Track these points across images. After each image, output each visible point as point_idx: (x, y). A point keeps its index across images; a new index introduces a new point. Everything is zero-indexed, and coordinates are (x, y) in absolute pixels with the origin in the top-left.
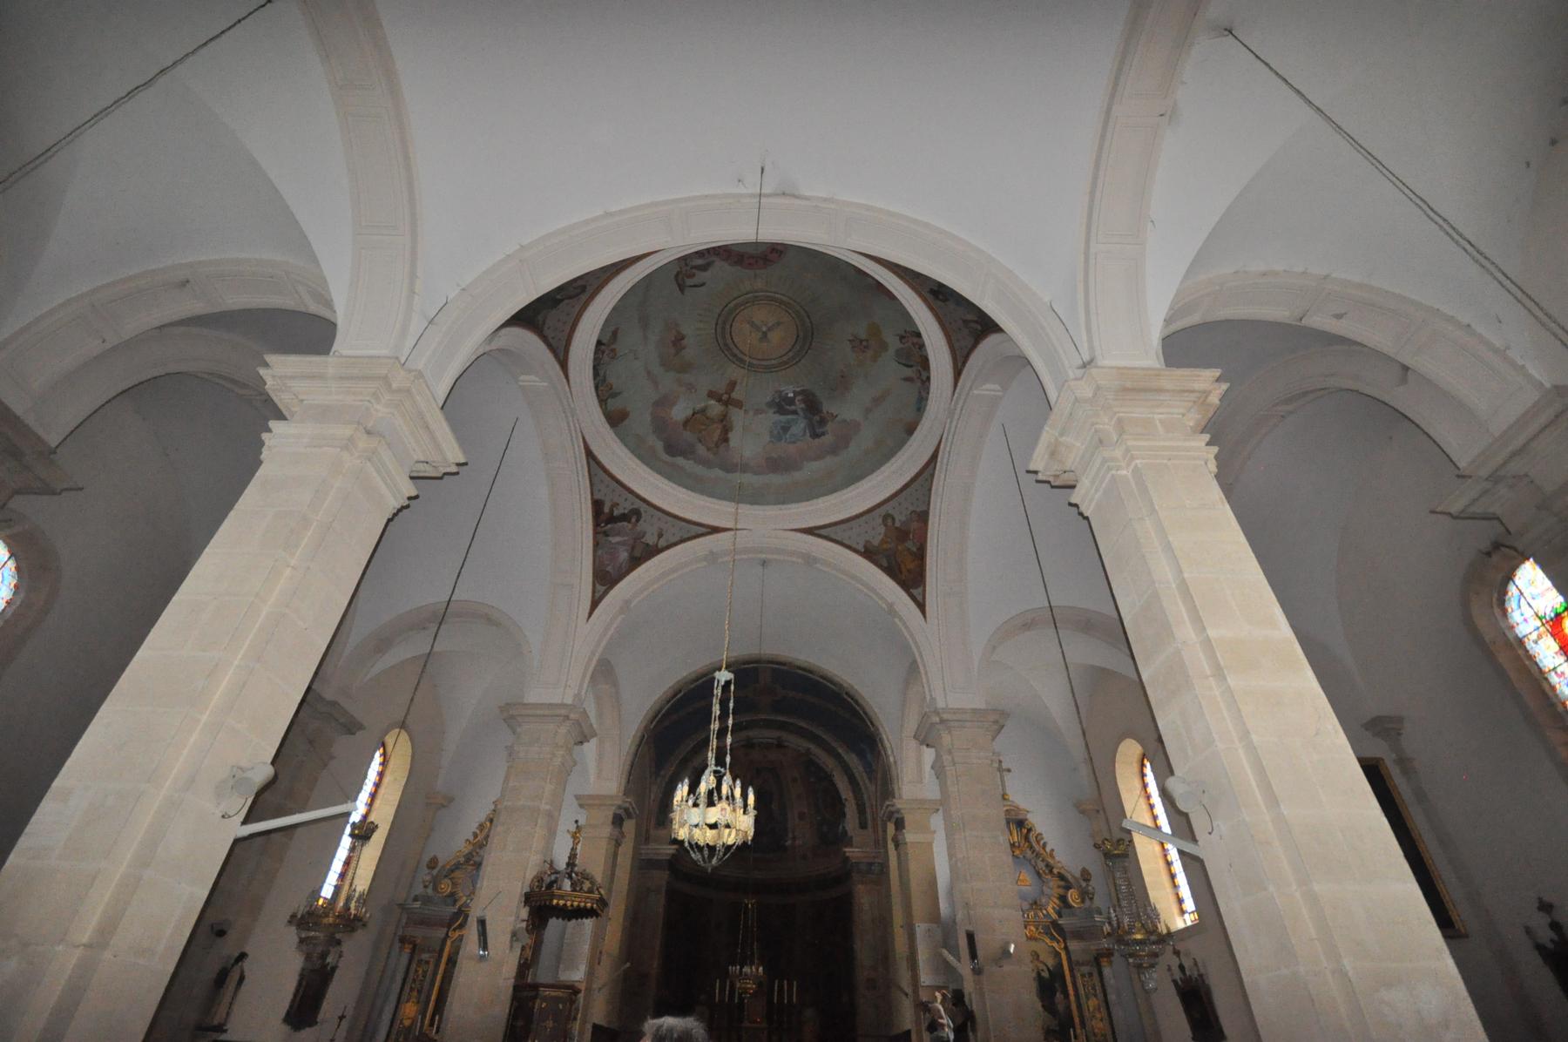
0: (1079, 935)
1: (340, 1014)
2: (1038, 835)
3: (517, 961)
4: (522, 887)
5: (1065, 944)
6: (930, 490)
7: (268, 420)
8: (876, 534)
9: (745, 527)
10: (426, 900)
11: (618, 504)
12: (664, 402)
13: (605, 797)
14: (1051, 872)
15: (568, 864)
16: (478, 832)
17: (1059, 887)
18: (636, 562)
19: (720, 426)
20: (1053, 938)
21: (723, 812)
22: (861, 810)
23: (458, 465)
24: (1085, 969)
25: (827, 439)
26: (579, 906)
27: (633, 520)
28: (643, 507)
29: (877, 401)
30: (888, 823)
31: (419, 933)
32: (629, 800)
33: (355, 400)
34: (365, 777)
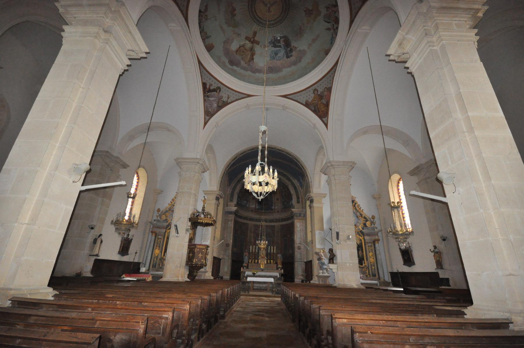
0: (368, 235)
1: (136, 252)
2: (358, 205)
3: (189, 237)
4: (188, 216)
5: (364, 237)
6: (333, 78)
7: (62, 26)
8: (310, 97)
9: (261, 95)
10: (158, 221)
11: (212, 85)
12: (227, 42)
13: (214, 191)
14: (362, 216)
15: (202, 210)
16: (172, 201)
17: (364, 221)
18: (220, 108)
20: (360, 235)
21: (266, 177)
22: (298, 198)
23: (147, 53)
24: (370, 244)
25: (293, 59)
26: (207, 222)
27: (218, 91)
28: (222, 86)
29: (314, 40)
30: (307, 201)
31: (157, 230)
32: (221, 192)
33: (97, 17)
34: (132, 183)
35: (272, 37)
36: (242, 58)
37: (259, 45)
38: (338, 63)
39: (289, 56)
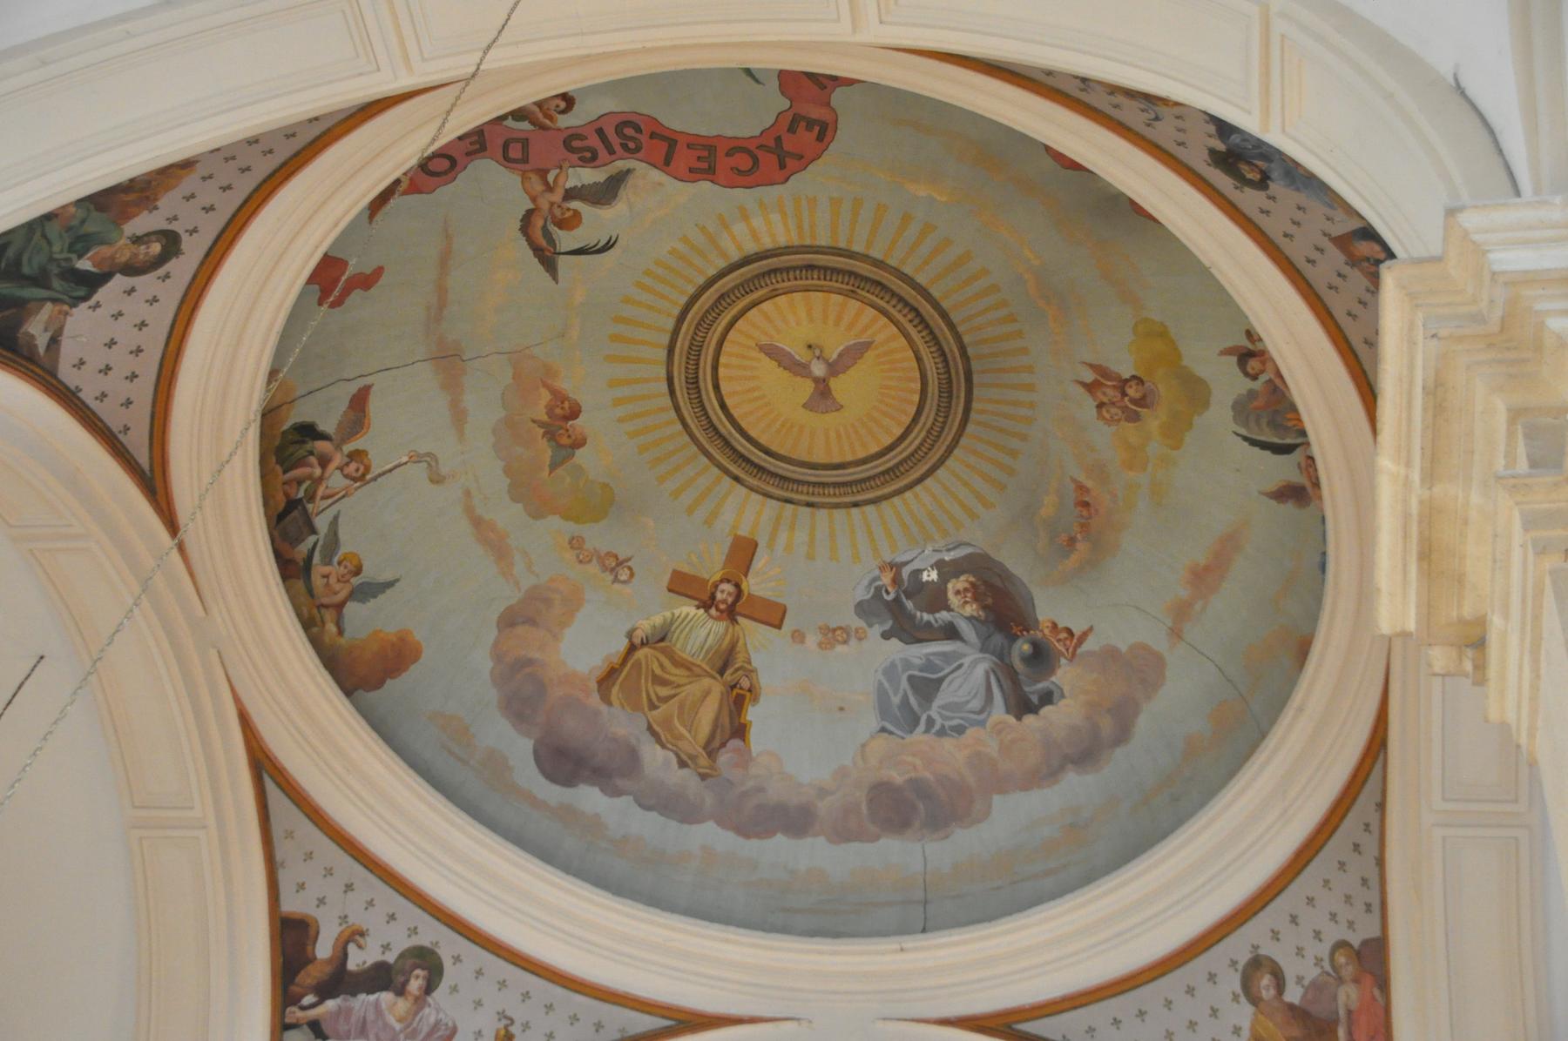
11: (362, 934)
19: (717, 688)
25: (1061, 717)
27: (415, 985)
28: (449, 945)
29: (1205, 578)
35: (882, 569)
36: (650, 728)
37: (779, 627)
38: (1383, 744)
39: (1035, 699)
